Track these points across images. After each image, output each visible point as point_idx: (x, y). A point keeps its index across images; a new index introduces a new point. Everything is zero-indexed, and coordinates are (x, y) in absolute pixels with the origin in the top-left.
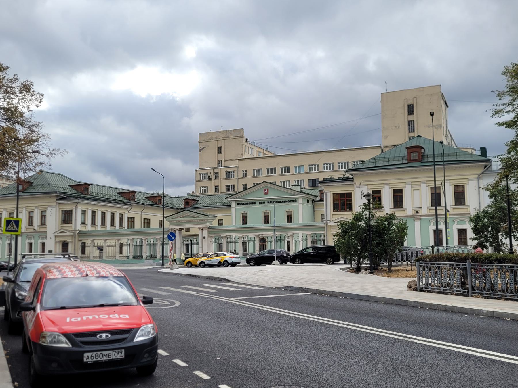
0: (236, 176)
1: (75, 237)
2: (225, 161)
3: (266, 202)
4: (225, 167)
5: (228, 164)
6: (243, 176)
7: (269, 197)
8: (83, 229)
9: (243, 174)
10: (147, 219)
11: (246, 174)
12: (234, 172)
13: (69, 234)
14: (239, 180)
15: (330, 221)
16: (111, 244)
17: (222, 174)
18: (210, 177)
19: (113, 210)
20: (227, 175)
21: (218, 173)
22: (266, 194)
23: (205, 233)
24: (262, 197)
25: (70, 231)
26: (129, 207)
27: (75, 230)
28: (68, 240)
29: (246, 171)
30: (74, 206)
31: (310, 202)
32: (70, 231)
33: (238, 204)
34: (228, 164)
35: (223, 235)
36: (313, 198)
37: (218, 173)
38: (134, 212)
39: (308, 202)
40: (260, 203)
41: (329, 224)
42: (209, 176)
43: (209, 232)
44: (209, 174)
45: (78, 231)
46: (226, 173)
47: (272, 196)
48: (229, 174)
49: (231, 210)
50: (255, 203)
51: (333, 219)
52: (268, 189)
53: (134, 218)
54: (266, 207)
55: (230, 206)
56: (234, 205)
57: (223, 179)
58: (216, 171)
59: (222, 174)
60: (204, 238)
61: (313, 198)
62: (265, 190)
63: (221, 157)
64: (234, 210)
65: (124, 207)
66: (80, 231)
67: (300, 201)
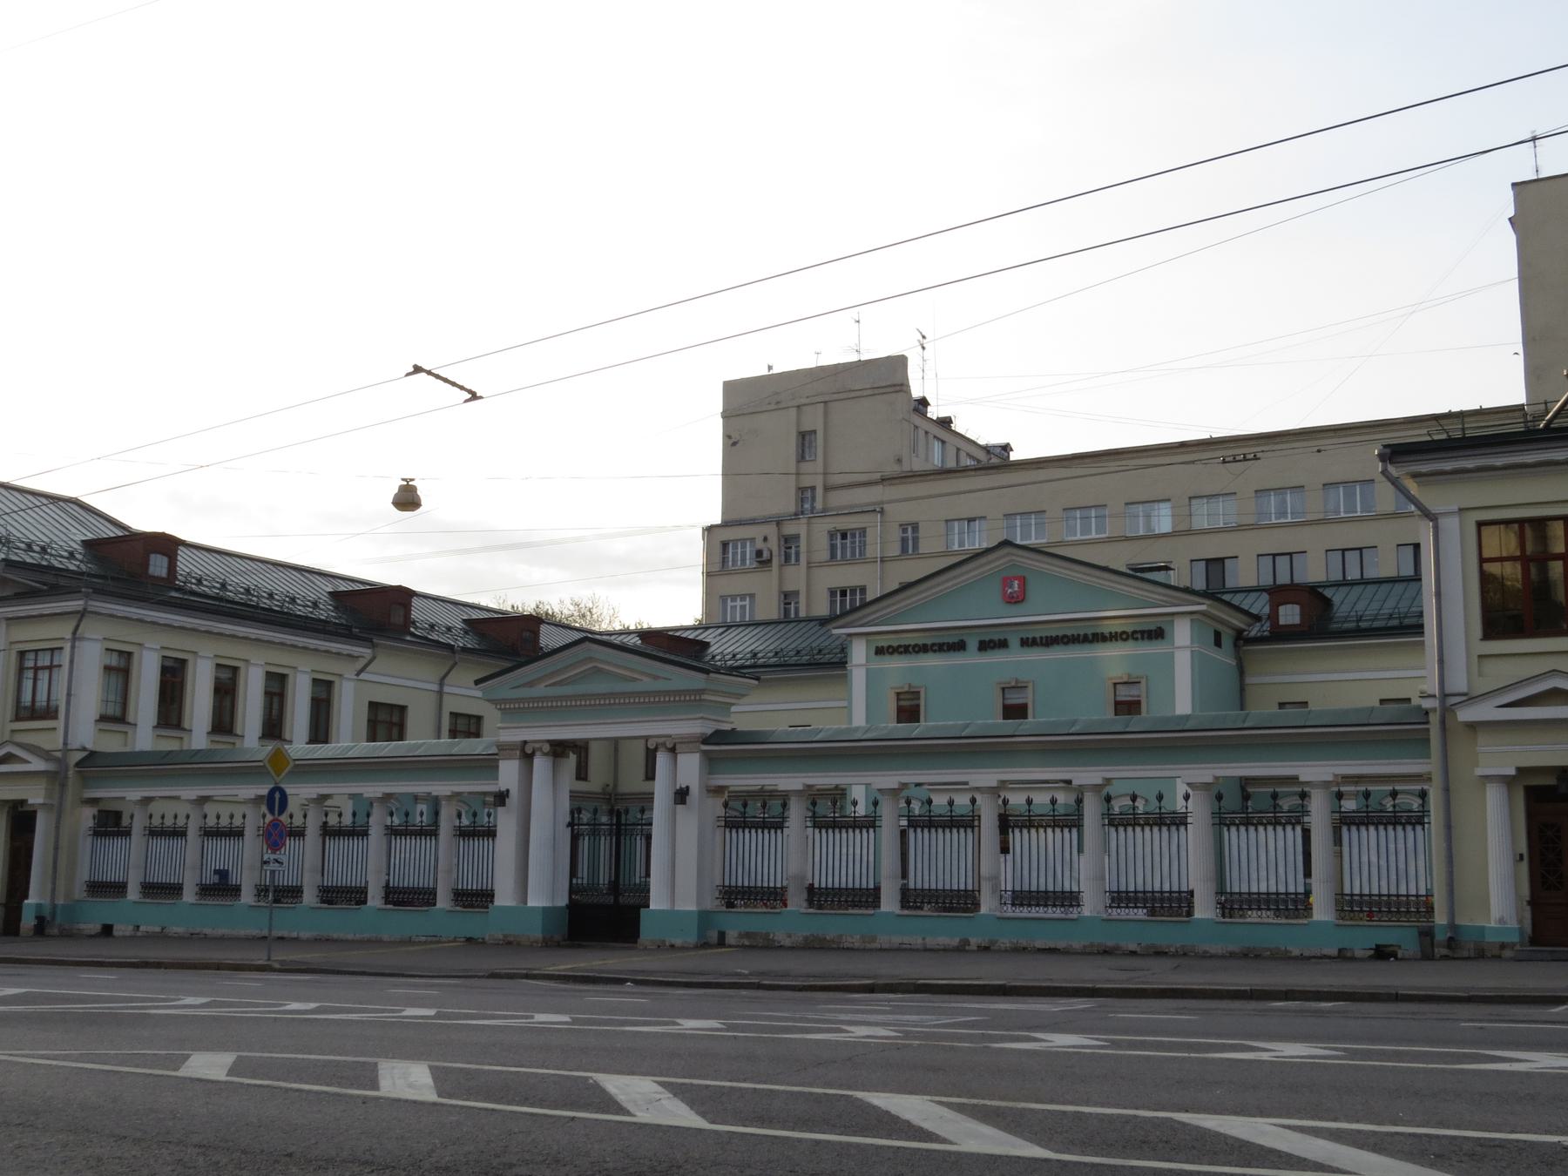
0: (873, 550)
1: (63, 786)
2: (827, 489)
3: (1014, 642)
4: (825, 512)
5: (840, 499)
6: (904, 550)
7: (1030, 614)
8: (111, 743)
9: (904, 541)
10: (469, 716)
11: (916, 540)
12: (863, 531)
13: (37, 765)
14: (887, 565)
15: (1470, 698)
16: (224, 822)
17: (815, 537)
18: (766, 555)
19: (281, 660)
20: (833, 548)
21: (797, 537)
22: (1016, 600)
23: (690, 769)
24: (990, 613)
25: (45, 755)
26: (366, 652)
27: (66, 749)
28: (35, 795)
29: (915, 527)
30: (64, 630)
31: (1227, 641)
32: (45, 755)
33: (880, 651)
34: (840, 499)
35: (789, 781)
36: (1237, 621)
37: (797, 537)
38: (397, 677)
39: (1218, 643)
40: (984, 646)
41: (1466, 715)
42: (759, 553)
43: (712, 763)
44: (760, 545)
45: (80, 756)
46: (832, 535)
47: (1041, 611)
48: (846, 542)
49: (845, 679)
50: (960, 646)
51: (1482, 686)
52: (1023, 581)
53: (403, 709)
54: (1015, 662)
55: (842, 664)
56: (859, 653)
57: (821, 565)
58: (790, 529)
59: (815, 537)
60: (681, 796)
61: (1237, 621)
62: (1007, 582)
63: (813, 474)
64: (858, 677)
65: (335, 646)
66: (92, 754)
67: (1182, 633)
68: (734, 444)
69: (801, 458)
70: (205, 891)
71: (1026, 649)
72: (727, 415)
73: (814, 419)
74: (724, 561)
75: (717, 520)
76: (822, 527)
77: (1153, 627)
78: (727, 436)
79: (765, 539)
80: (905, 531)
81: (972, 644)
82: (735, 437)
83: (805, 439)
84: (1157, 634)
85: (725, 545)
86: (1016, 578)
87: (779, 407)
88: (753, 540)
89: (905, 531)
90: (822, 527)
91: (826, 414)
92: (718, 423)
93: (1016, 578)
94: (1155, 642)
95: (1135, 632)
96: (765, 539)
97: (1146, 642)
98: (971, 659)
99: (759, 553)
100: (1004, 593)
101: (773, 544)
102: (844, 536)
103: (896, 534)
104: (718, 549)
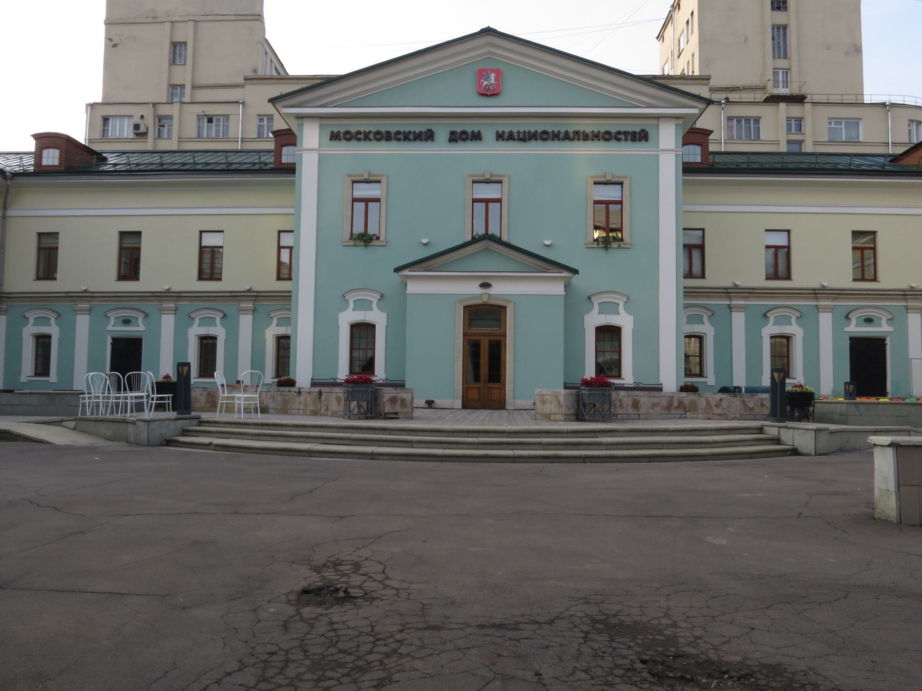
2: (194, 87)
3: (489, 134)
5: (203, 95)
18: (142, 129)
22: (489, 93)
33: (335, 137)
34: (203, 95)
37: (170, 117)
40: (454, 138)
46: (200, 118)
50: (429, 136)
54: (488, 154)
58: (164, 110)
62: (482, 74)
63: (183, 75)
68: (115, 46)
69: (173, 62)
70: (162, 387)
71: (501, 143)
72: (109, 23)
73: (184, 33)
74: (105, 131)
75: (99, 100)
76: (193, 111)
77: (638, 130)
78: (109, 39)
79: (142, 117)
80: (261, 120)
81: (442, 135)
82: (116, 40)
83: (177, 48)
84: (641, 136)
85: (106, 119)
86: (492, 71)
87: (155, 21)
88: (130, 116)
89: (261, 120)
90: (193, 111)
91: (195, 31)
92: (101, 29)
93: (492, 71)
94: (638, 144)
95: (619, 133)
96: (142, 117)
97: (629, 143)
98: (440, 149)
99: (137, 127)
100: (480, 86)
101: (149, 121)
102: (210, 120)
103: (255, 122)
104: (100, 122)
